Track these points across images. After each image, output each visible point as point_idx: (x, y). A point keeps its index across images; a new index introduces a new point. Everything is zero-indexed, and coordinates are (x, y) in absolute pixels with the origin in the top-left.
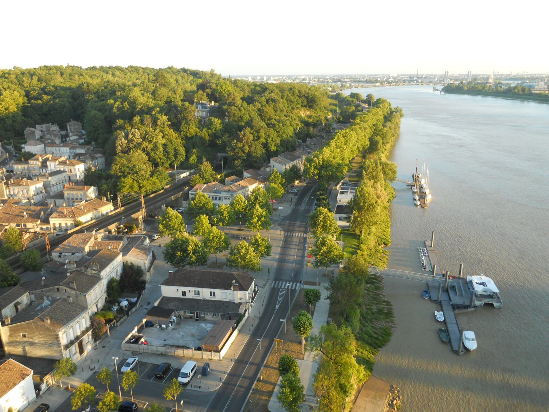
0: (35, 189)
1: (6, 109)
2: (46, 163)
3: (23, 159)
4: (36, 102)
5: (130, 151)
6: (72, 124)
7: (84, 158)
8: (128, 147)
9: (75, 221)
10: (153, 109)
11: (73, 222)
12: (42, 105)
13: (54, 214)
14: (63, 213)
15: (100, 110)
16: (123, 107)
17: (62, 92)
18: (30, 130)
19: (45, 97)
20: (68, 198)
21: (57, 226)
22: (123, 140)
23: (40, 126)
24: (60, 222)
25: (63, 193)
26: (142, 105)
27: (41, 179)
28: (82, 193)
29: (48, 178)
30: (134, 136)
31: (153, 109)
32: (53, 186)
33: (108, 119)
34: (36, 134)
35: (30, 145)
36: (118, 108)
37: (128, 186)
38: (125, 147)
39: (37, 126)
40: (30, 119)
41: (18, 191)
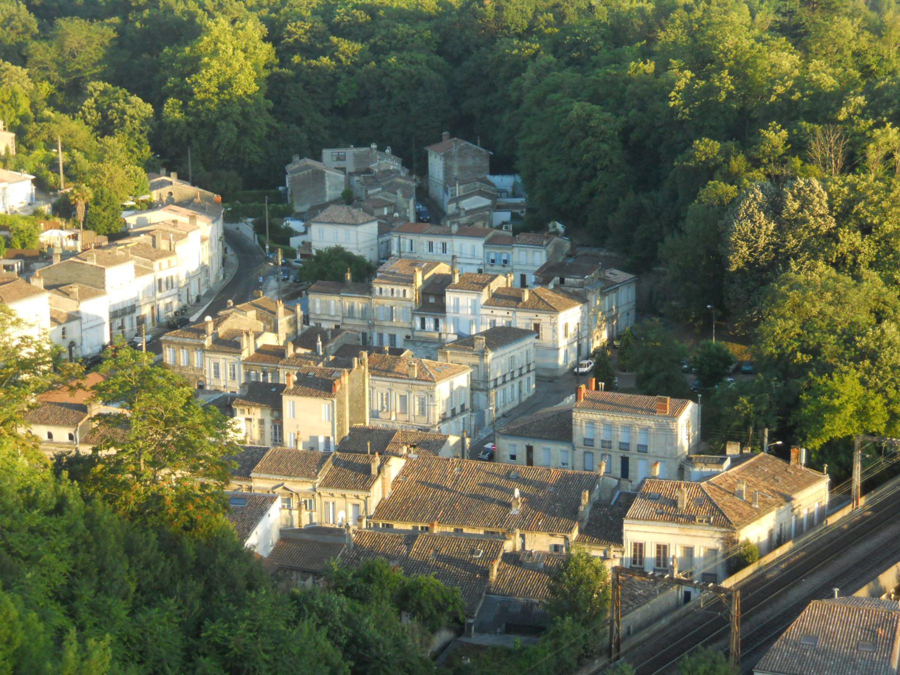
0: (448, 395)
1: (222, 87)
2: (443, 295)
3: (349, 276)
4: (314, 62)
5: (787, 267)
6: (455, 150)
7: (581, 285)
8: (775, 251)
9: (729, 541)
10: (839, 98)
11: (718, 546)
12: (333, 75)
13: (638, 507)
14: (674, 503)
15: (595, 99)
16: (711, 90)
17: (402, 29)
18: (307, 167)
19: (347, 47)
20: (589, 442)
21: (650, 553)
22: (761, 217)
23: (335, 151)
24: (663, 540)
25: (570, 420)
26: (790, 83)
27: (455, 358)
28: (649, 422)
29: (482, 354)
30: (806, 203)
31: (839, 98)
32: (496, 386)
33: (634, 136)
34: (328, 183)
35: (333, 223)
36: (688, 94)
37: (851, 409)
38: (766, 249)
39: (327, 153)
40: (294, 127)
41: (387, 399)
